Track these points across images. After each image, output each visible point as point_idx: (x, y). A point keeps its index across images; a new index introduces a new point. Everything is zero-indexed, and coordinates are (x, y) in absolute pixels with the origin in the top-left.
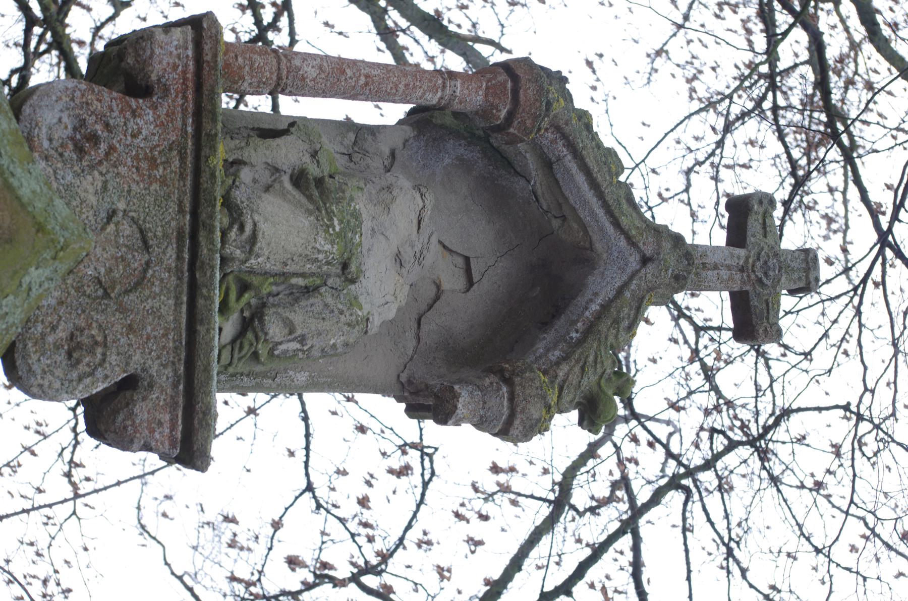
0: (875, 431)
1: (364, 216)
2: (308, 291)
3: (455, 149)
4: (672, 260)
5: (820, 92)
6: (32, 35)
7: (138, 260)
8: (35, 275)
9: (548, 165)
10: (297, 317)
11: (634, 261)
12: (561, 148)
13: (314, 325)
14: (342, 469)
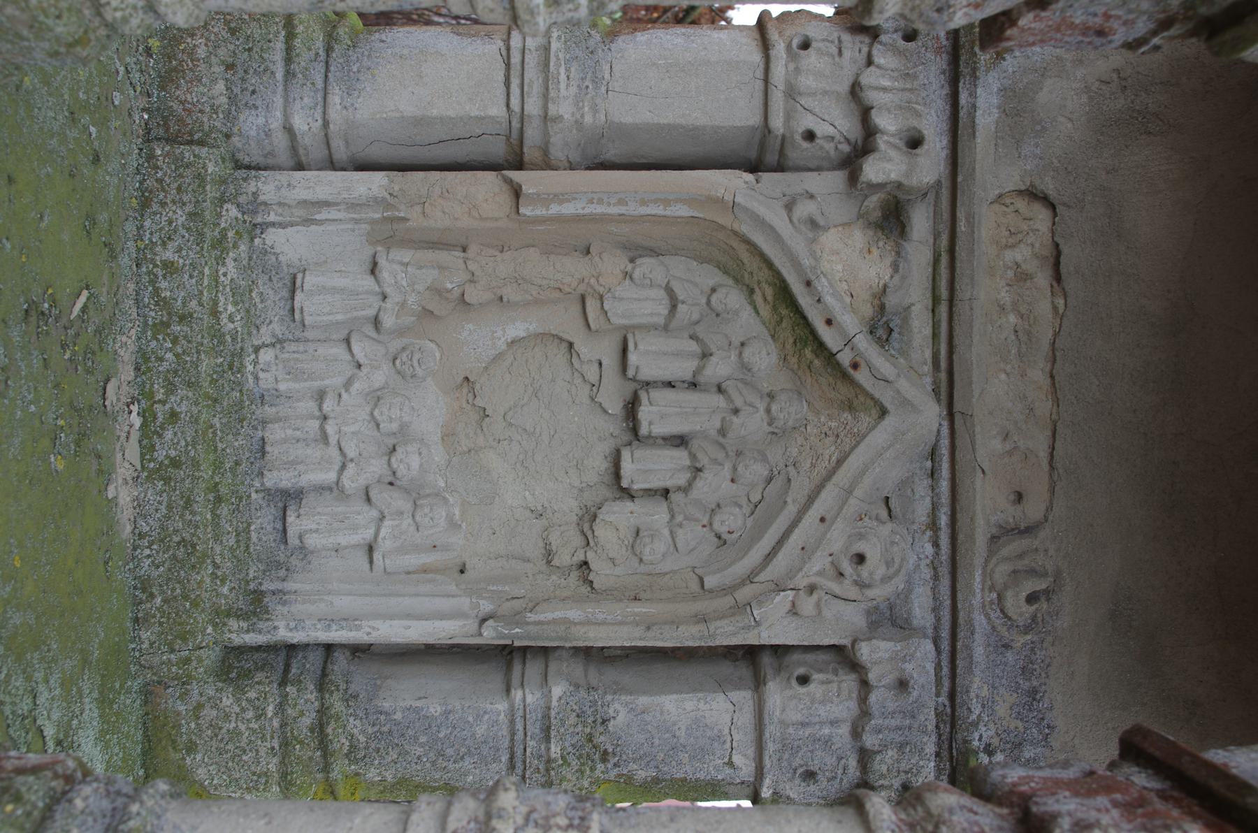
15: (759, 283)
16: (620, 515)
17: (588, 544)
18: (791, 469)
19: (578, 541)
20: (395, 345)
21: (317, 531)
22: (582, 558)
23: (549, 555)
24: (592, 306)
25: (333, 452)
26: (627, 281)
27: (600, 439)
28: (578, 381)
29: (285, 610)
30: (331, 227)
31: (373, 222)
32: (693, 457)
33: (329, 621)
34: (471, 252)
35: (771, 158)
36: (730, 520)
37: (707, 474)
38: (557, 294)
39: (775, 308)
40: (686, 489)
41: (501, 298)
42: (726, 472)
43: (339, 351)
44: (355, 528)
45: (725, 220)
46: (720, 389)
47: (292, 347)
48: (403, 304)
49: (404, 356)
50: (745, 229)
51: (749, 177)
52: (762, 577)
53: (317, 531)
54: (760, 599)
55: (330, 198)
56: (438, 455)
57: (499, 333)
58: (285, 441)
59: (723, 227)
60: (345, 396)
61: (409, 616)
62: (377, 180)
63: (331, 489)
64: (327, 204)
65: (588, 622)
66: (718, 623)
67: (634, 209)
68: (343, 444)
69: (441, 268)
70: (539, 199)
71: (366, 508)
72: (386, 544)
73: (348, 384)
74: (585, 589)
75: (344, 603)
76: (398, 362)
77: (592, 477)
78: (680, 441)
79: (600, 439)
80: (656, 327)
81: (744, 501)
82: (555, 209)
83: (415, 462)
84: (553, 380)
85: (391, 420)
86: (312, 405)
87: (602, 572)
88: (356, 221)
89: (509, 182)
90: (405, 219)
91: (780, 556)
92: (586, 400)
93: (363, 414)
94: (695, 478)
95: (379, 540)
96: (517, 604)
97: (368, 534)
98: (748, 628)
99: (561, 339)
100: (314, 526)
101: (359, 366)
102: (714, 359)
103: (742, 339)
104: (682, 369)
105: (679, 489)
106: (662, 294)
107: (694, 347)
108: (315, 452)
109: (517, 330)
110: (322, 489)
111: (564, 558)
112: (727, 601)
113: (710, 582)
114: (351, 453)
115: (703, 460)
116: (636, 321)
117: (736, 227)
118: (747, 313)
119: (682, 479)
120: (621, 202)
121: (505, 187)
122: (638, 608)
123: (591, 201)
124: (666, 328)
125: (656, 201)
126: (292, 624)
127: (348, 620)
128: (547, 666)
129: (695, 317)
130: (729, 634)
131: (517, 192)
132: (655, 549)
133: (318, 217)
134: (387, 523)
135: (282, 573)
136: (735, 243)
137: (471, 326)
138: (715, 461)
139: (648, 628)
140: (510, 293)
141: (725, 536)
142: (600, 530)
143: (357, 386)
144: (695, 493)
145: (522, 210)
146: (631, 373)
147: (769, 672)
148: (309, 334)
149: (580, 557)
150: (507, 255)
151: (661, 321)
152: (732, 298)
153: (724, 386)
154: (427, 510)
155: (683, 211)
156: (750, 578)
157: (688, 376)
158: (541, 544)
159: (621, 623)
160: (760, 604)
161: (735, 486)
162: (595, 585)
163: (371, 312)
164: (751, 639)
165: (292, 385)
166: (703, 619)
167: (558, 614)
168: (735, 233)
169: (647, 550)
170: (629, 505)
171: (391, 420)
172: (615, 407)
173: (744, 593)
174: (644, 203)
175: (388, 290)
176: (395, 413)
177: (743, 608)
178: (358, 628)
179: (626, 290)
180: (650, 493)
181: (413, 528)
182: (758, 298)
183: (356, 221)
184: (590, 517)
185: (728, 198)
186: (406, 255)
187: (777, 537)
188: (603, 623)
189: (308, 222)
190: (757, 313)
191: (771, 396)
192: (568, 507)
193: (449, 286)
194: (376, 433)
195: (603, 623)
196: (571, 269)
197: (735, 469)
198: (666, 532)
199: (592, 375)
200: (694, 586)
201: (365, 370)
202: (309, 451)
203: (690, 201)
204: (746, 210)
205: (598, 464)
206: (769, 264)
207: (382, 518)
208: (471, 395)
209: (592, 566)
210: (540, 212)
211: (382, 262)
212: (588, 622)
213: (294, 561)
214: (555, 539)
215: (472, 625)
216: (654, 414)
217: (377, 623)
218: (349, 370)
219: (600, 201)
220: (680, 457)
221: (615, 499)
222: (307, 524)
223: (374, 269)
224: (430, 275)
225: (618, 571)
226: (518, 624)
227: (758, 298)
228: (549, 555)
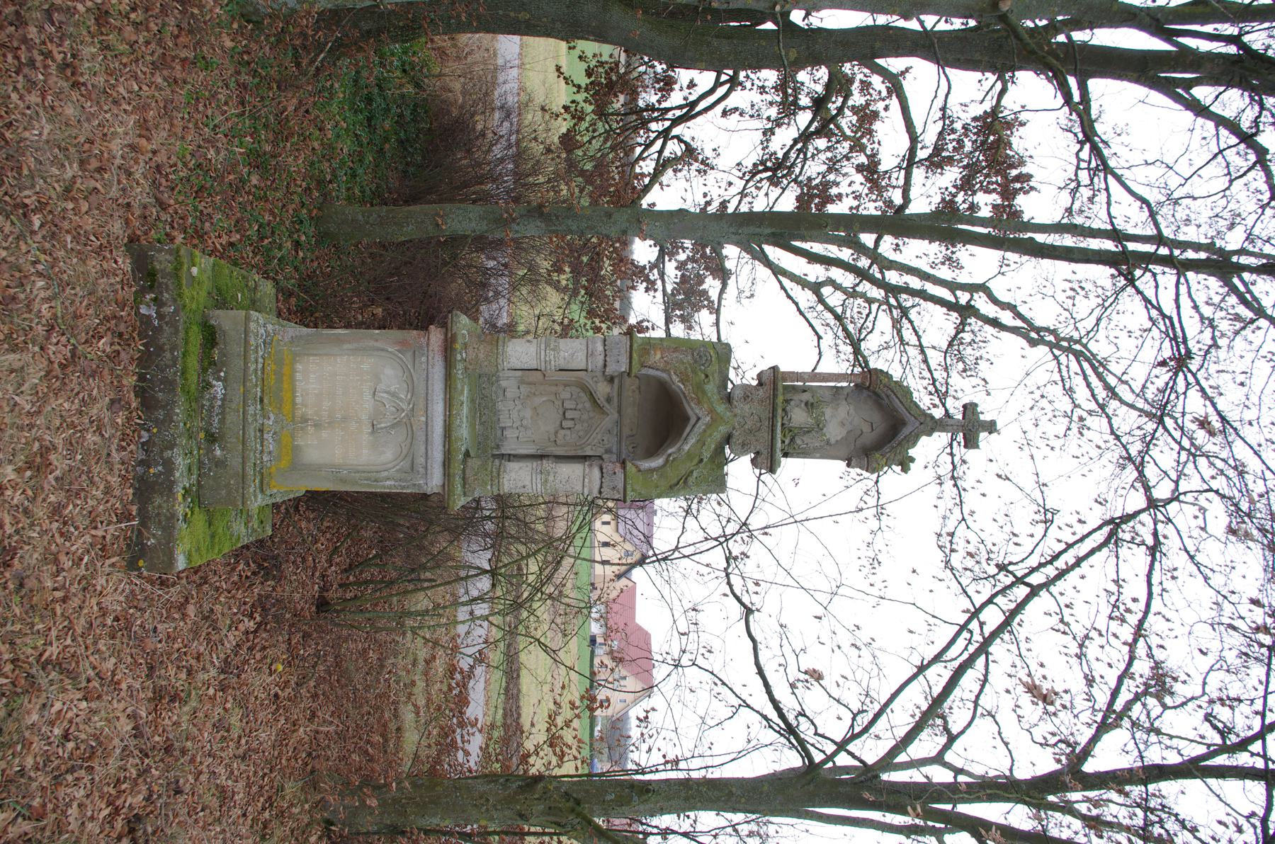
0: (973, 610)
1: (716, 397)
2: (808, 432)
3: (865, 393)
4: (930, 424)
5: (662, 811)
6: (689, 339)
7: (758, 425)
8: (721, 428)
9: (888, 396)
10: (804, 438)
11: (917, 424)
12: (890, 392)
13: (810, 441)
14: (1215, 324)
16: (562, 432)
36: (581, 433)
62: (519, 373)
75: (513, 447)
78: (573, 419)
87: (558, 442)
104: (573, 407)
130: (580, 453)
132: (567, 438)
152: (582, 394)
184: (556, 432)
192: (553, 431)
196: (554, 389)
205: (558, 423)
216: (569, 415)
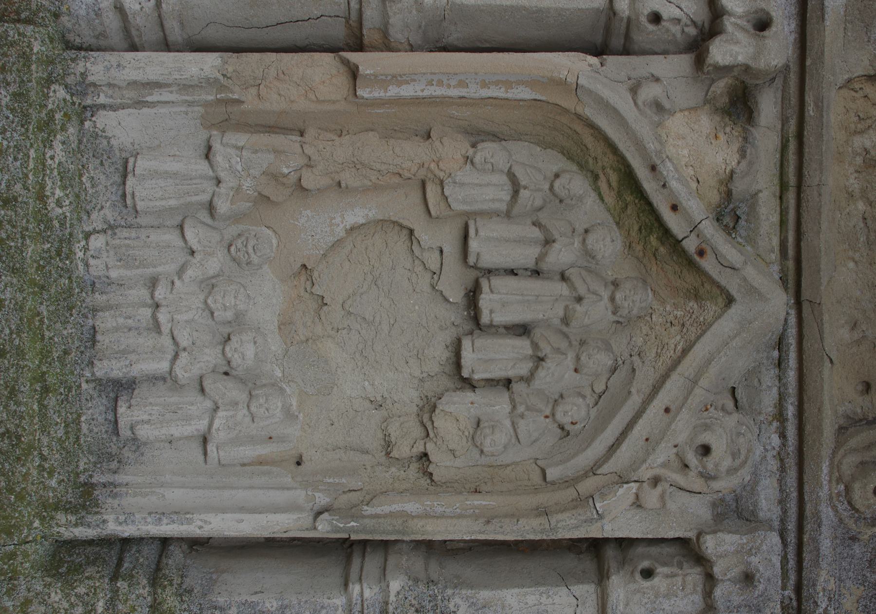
15: (603, 168)
17: (428, 435)
18: (635, 358)
19: (418, 432)
20: (232, 231)
21: (148, 422)
22: (421, 449)
23: (388, 446)
24: (432, 191)
25: (166, 341)
26: (468, 166)
27: (441, 328)
28: (419, 269)
29: (116, 502)
30: (163, 110)
31: (206, 104)
32: (535, 346)
33: (160, 515)
34: (308, 137)
35: (617, 42)
37: (549, 364)
38: (396, 180)
39: (619, 195)
40: (528, 379)
41: (339, 184)
42: (570, 361)
43: (172, 237)
44: (188, 419)
45: (568, 103)
46: (563, 277)
47: (125, 233)
48: (238, 189)
49: (239, 243)
50: (588, 112)
51: (594, 60)
52: (605, 469)
53: (148, 422)
54: (603, 491)
55: (160, 79)
56: (275, 344)
57: (338, 220)
58: (116, 329)
59: (566, 111)
60: (178, 283)
61: (242, 509)
62: (210, 62)
63: (164, 379)
64: (157, 85)
65: (426, 516)
66: (560, 516)
67: (474, 91)
68: (175, 333)
69: (277, 152)
70: (376, 81)
71: (200, 398)
72: (219, 435)
73: (181, 271)
74: (424, 482)
75: (176, 496)
76: (233, 249)
77: (433, 367)
78: (523, 330)
79: (441, 328)
80: (497, 214)
81: (588, 392)
82: (393, 91)
83: (250, 351)
84: (393, 268)
85: (225, 308)
86: (144, 293)
88: (190, 104)
89: (346, 63)
90: (239, 102)
91: (624, 447)
92: (427, 288)
93: (197, 302)
94: (537, 367)
95: (213, 431)
96: (354, 497)
97: (202, 425)
98: (591, 521)
99: (402, 226)
100: (146, 417)
101: (193, 253)
102: (556, 246)
103: (585, 226)
105: (522, 379)
106: (504, 179)
107: (536, 233)
108: (146, 341)
109: (356, 216)
110: (155, 379)
111: (403, 450)
112: (570, 493)
113: (553, 473)
114: (184, 342)
115: (546, 349)
116: (476, 207)
117: (579, 110)
118: (591, 199)
119: (524, 369)
120: (462, 84)
121: (343, 69)
122: (478, 501)
123: (430, 83)
124: (508, 215)
125: (497, 83)
126: (122, 518)
127: (179, 513)
128: (386, 560)
129: (538, 203)
131: (354, 73)
133: (149, 99)
134: (220, 414)
135: (114, 465)
136: (578, 127)
137: (308, 212)
138: (558, 351)
139: (488, 522)
140: (348, 178)
141: (568, 427)
142: (440, 422)
143: (190, 273)
144: (537, 383)
145: (360, 92)
146: (472, 260)
147: (613, 565)
148: (142, 220)
149: (419, 448)
150: (346, 139)
151: (503, 207)
153: (567, 273)
154: (262, 401)
155: (525, 93)
156: (592, 471)
157: (531, 264)
158: (380, 435)
159: (460, 516)
160: (603, 496)
161: (578, 376)
162: (435, 478)
163: (205, 197)
164: (594, 532)
165: (123, 272)
166: (544, 512)
167: (396, 507)
168: (579, 116)
169: (488, 441)
170: (469, 396)
171: (225, 308)
172: (456, 295)
173: (587, 486)
174: (484, 85)
175: (222, 175)
176: (230, 301)
177: (585, 501)
178: (190, 522)
179: (466, 175)
180: (492, 383)
181: (248, 419)
182: (603, 184)
183: (190, 104)
185: (571, 79)
186: (241, 139)
187: (617, 434)
188: (442, 516)
189: (139, 104)
190: (602, 199)
191: (616, 284)
193: (286, 171)
194: (210, 322)
195: (442, 516)
197: (578, 358)
198: (507, 423)
199: (433, 260)
200: (536, 478)
201: (198, 257)
202: (141, 340)
203: (532, 83)
204: (590, 92)
205: (439, 353)
206: (613, 148)
207: (216, 409)
208: (309, 283)
209: (432, 458)
210: (378, 93)
211: (217, 146)
212: (426, 516)
213: (126, 453)
214: (394, 431)
215: (306, 519)
217: (210, 517)
218: (182, 257)
219: (440, 83)
220: (523, 345)
221: (456, 389)
222: (139, 414)
223: (208, 153)
224: (265, 160)
225: (458, 463)
226: (353, 517)
227: (603, 184)
228: (388, 446)
